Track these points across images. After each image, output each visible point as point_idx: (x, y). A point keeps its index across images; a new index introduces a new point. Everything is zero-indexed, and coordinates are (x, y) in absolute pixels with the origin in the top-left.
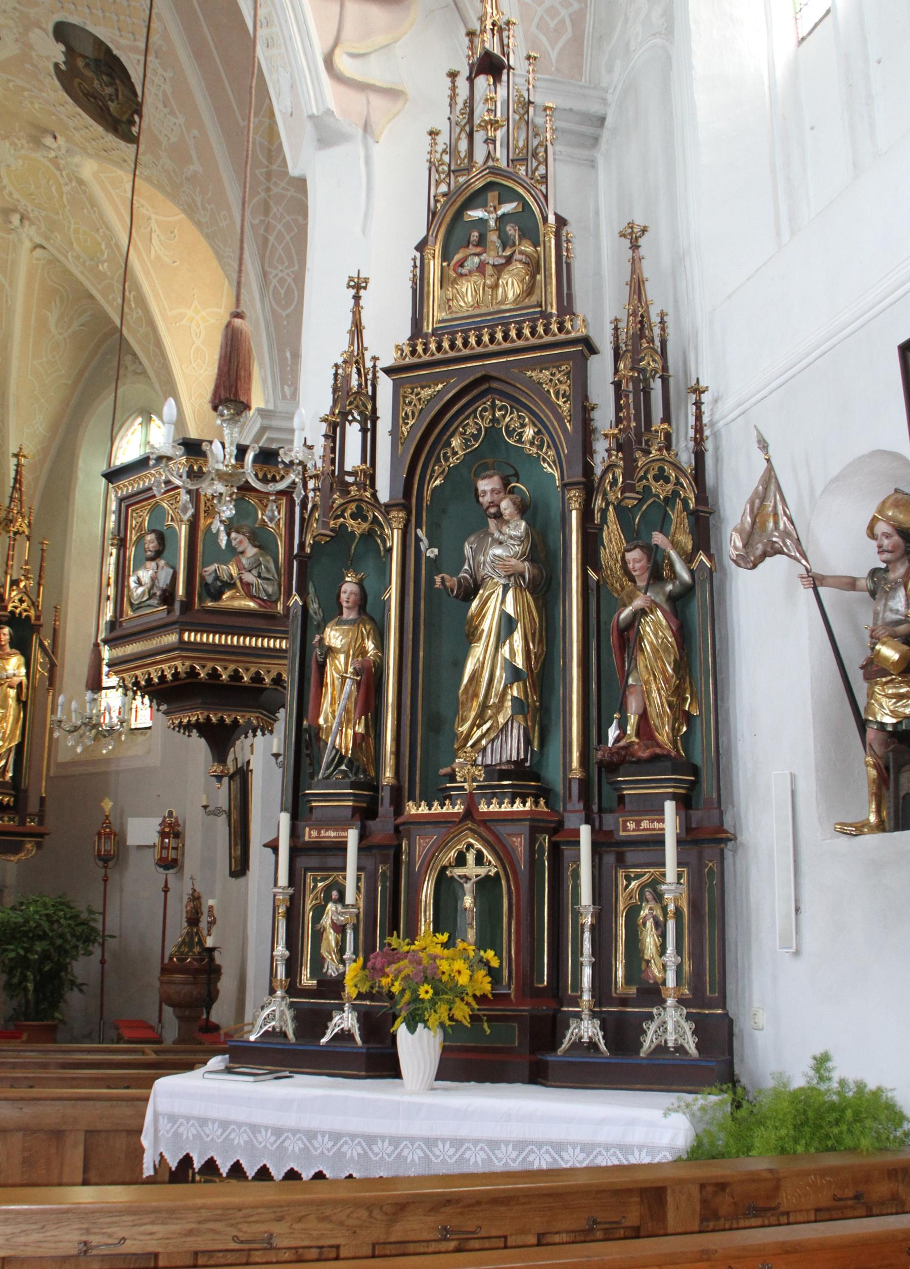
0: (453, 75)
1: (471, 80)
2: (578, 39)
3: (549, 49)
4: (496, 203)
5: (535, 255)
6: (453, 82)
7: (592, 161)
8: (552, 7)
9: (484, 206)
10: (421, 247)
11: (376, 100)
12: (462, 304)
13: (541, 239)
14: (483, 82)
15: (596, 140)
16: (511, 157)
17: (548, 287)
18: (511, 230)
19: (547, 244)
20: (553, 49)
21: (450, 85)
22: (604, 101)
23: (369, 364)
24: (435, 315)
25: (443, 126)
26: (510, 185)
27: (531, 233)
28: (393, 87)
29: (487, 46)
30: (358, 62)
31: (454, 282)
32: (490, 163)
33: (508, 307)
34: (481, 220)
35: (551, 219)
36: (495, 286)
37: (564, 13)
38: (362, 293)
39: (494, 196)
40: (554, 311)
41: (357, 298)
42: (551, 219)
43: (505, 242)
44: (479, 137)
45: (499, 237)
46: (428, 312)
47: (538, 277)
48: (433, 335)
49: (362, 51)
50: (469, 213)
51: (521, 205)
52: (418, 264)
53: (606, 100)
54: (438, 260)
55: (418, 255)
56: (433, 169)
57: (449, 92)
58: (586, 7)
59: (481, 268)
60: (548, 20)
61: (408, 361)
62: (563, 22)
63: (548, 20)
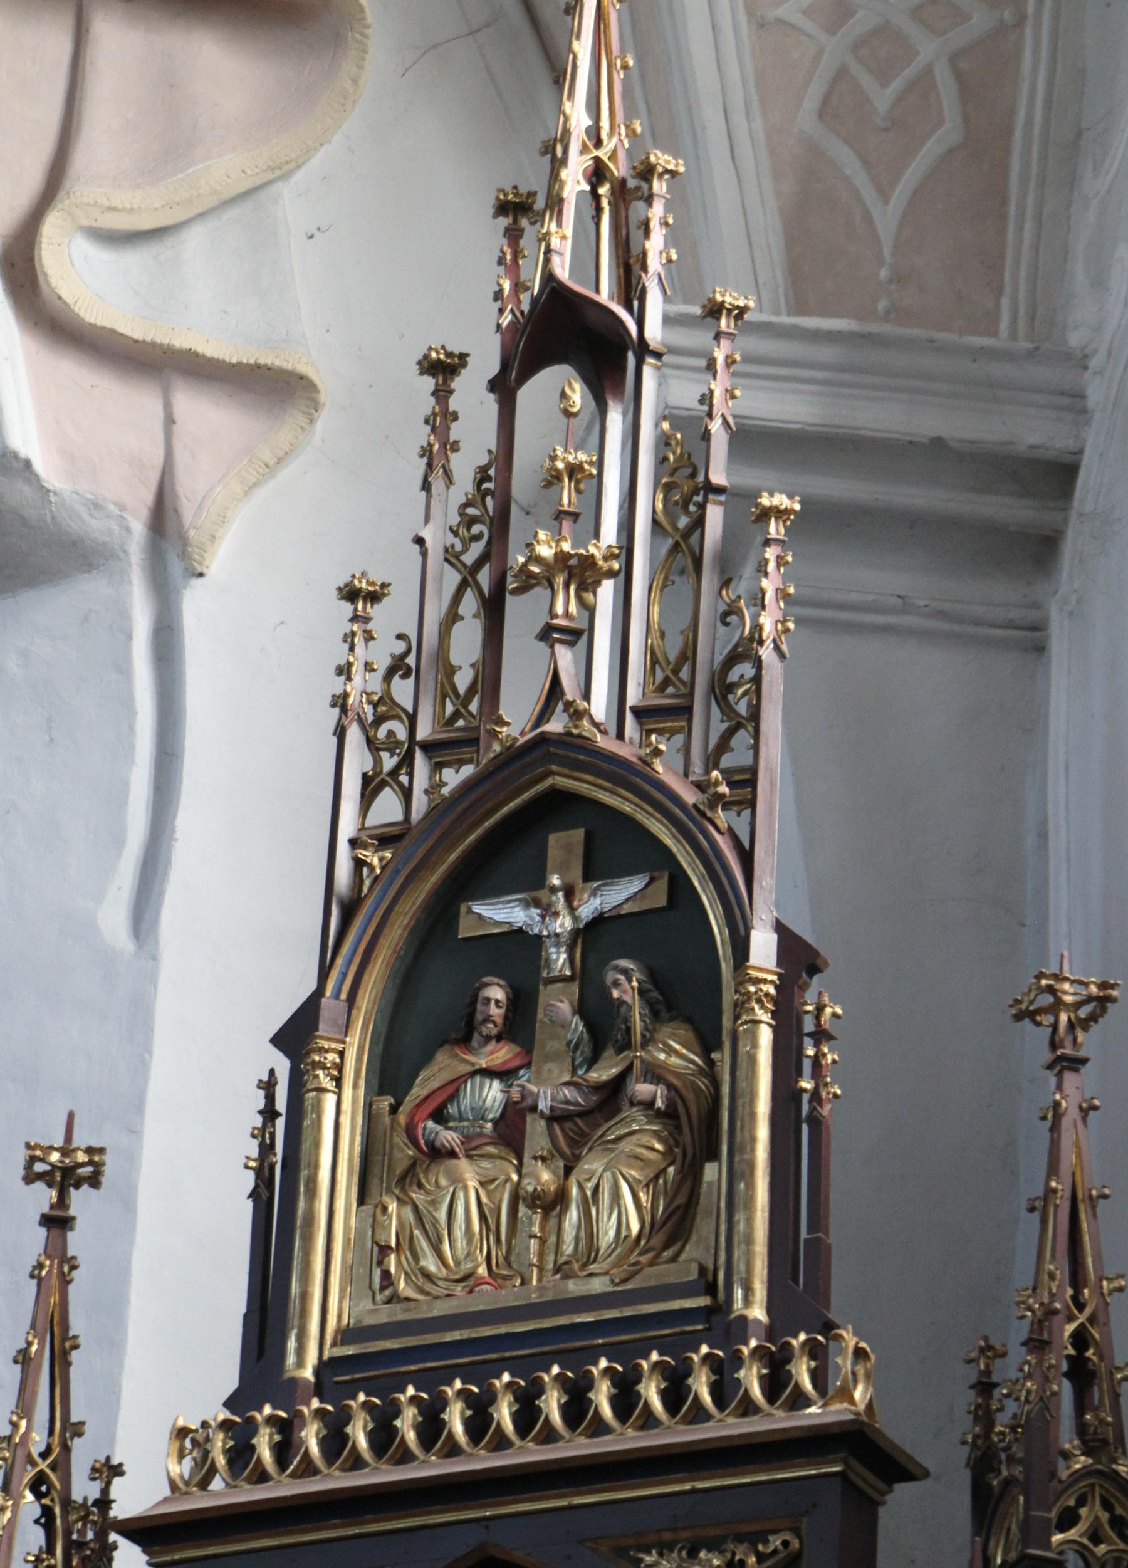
0: (443, 369)
1: (504, 387)
2: (984, 148)
3: (868, 192)
4: (576, 873)
5: (702, 1083)
6: (442, 394)
7: (1034, 628)
8: (883, 31)
9: (529, 884)
10: (296, 1036)
11: (202, 413)
12: (430, 1264)
13: (726, 1022)
14: (558, 387)
15: (1041, 550)
16: (633, 696)
17: (740, 1216)
18: (626, 985)
19: (744, 1048)
20: (885, 196)
21: (428, 404)
22: (1073, 404)
23: (84, 1489)
24: (329, 1304)
25: (397, 569)
26: (627, 808)
27: (692, 993)
28: (266, 359)
29: (562, 270)
30: (133, 261)
31: (408, 1178)
32: (556, 725)
33: (598, 1285)
34: (517, 935)
35: (763, 947)
36: (552, 1204)
37: (929, 50)
38: (80, 1200)
39: (568, 848)
40: (758, 1313)
41: (57, 1222)
42: (763, 947)
43: (602, 1027)
44: (522, 614)
45: (581, 1009)
46: (305, 1296)
47: (710, 1171)
48: (319, 1389)
49: (146, 223)
50: (478, 908)
51: (662, 885)
52: (281, 1105)
53: (1082, 396)
54: (353, 1096)
55: (283, 1065)
56: (354, 734)
57: (423, 435)
58: (1021, 20)
59: (510, 1130)
60: (866, 80)
61: (221, 1492)
62: (924, 84)
63: (866, 80)
